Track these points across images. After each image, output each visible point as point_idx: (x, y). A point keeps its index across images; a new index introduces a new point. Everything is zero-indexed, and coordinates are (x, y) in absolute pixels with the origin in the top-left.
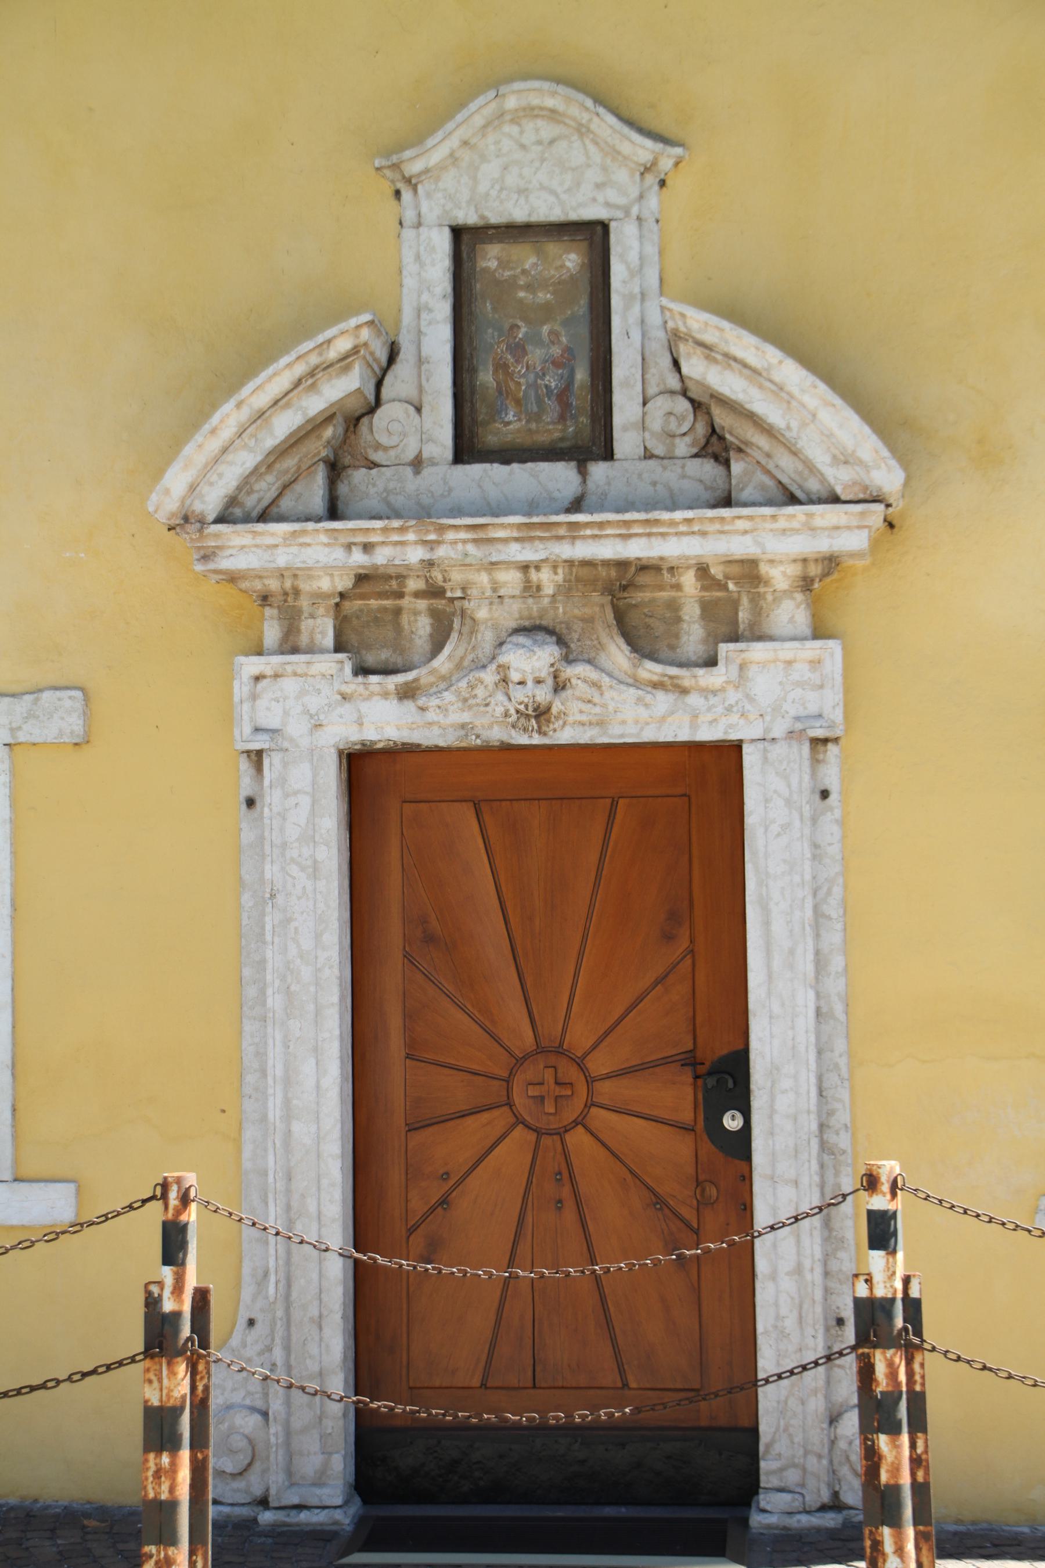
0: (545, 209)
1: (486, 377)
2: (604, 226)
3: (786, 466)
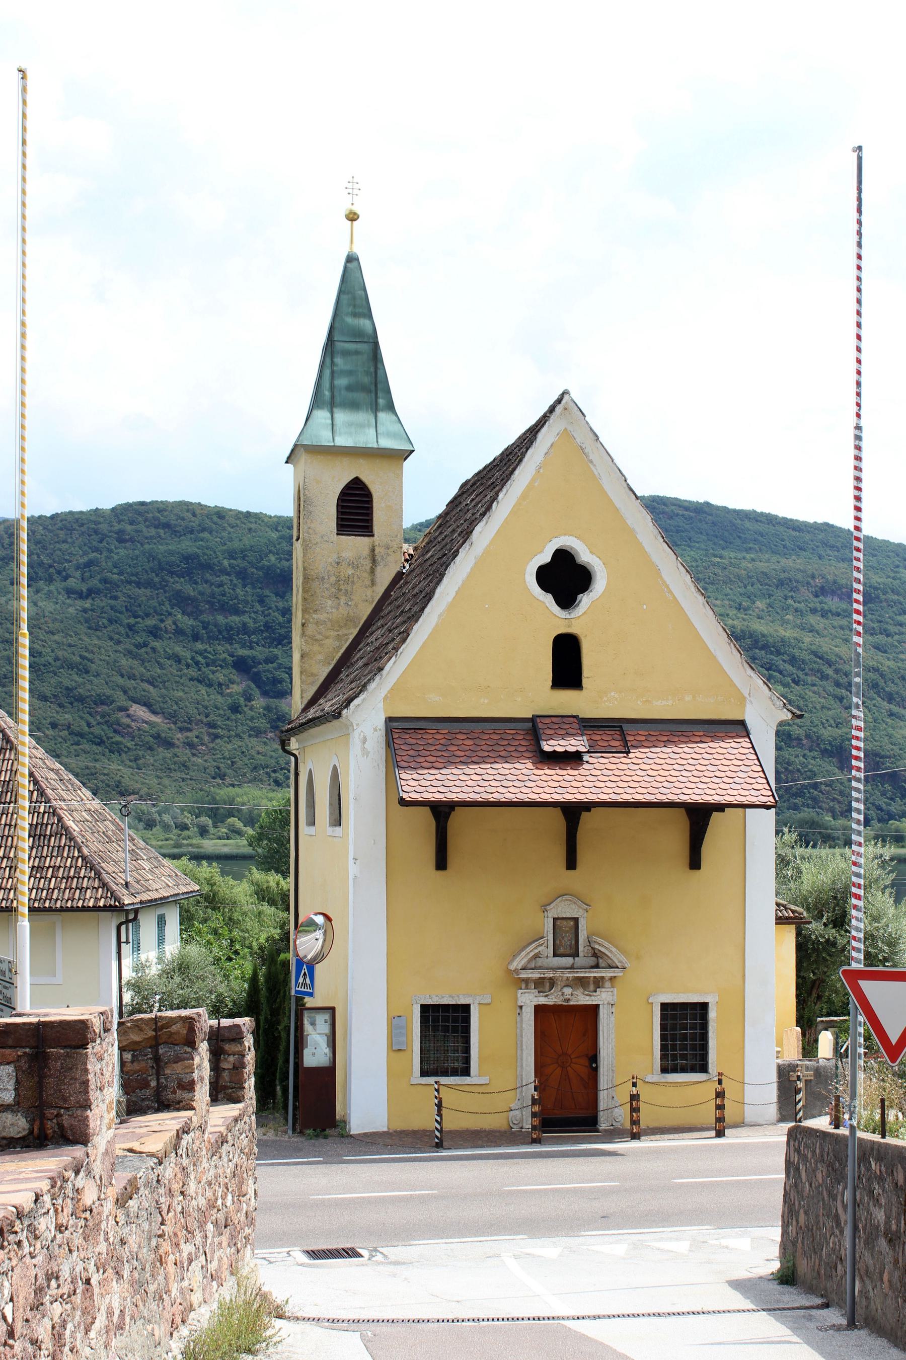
1: (558, 942)
3: (610, 962)
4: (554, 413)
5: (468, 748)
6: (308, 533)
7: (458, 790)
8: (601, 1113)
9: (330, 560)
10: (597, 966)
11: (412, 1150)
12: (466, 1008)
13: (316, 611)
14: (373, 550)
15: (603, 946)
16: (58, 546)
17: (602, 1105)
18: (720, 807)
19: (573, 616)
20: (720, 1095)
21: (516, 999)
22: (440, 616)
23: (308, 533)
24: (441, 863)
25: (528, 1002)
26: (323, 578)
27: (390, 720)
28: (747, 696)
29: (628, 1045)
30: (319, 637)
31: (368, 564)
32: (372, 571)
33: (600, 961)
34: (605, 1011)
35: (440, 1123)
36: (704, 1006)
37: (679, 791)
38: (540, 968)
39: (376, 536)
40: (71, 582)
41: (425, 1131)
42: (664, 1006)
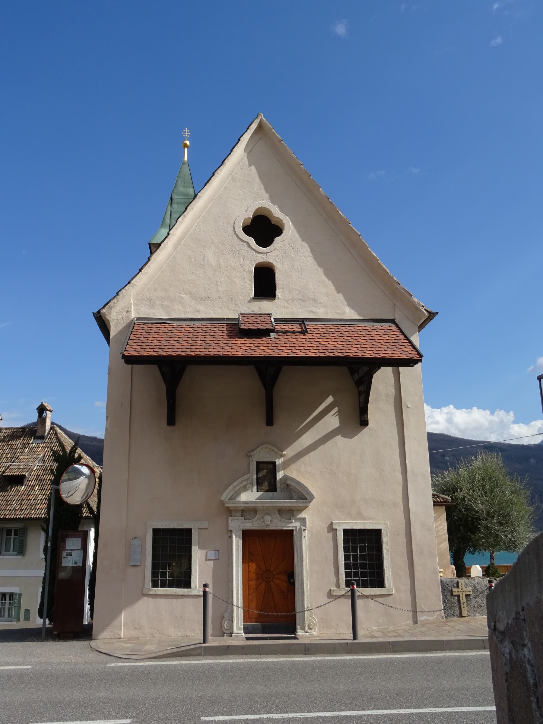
24: (171, 421)
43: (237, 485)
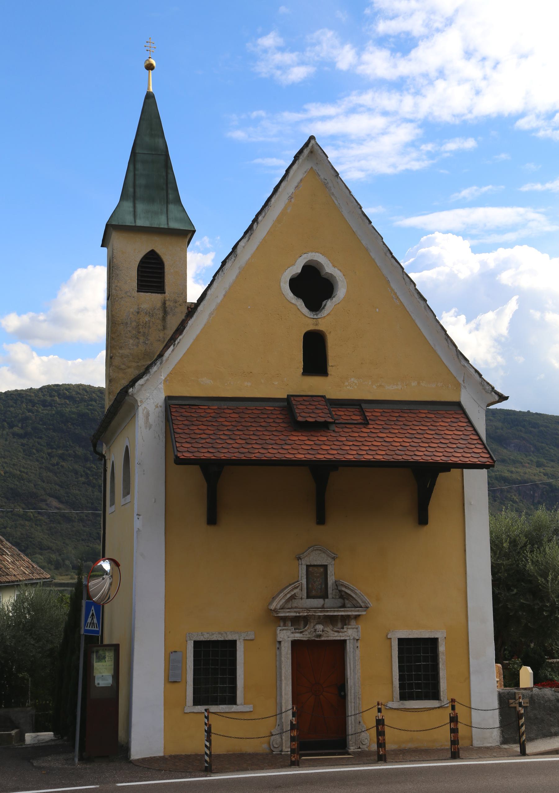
0: (319, 563)
1: (310, 586)
2: (327, 565)
3: (354, 602)
4: (303, 154)
5: (234, 419)
6: (116, 290)
7: (226, 451)
8: (350, 737)
9: (132, 310)
10: (343, 606)
11: (183, 774)
12: (233, 643)
13: (121, 348)
14: (164, 303)
15: (349, 588)
16: (8, 409)
17: (351, 729)
18: (446, 467)
19: (319, 316)
20: (454, 719)
21: (275, 635)
22: (211, 314)
23: (116, 290)
25: (286, 638)
26: (127, 323)
27: (168, 398)
28: (461, 382)
29: (370, 677)
30: (123, 367)
31: (160, 314)
32: (164, 319)
33: (347, 602)
34: (351, 646)
35: (209, 748)
36: (434, 641)
37: (412, 453)
38: (296, 608)
39: (167, 294)
40: (16, 429)
41: (197, 755)
42: (401, 641)
43: (288, 593)
